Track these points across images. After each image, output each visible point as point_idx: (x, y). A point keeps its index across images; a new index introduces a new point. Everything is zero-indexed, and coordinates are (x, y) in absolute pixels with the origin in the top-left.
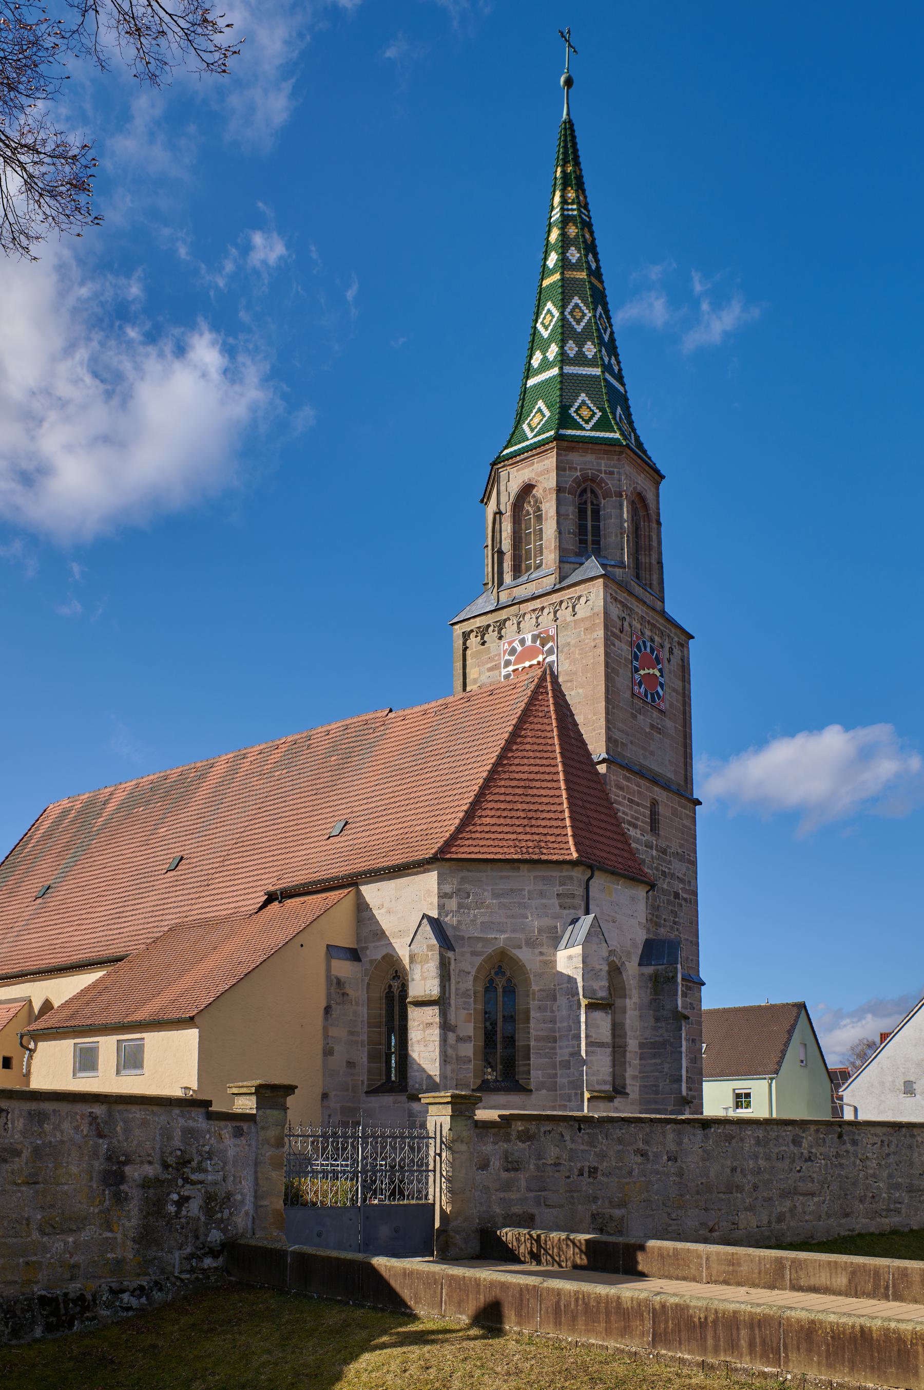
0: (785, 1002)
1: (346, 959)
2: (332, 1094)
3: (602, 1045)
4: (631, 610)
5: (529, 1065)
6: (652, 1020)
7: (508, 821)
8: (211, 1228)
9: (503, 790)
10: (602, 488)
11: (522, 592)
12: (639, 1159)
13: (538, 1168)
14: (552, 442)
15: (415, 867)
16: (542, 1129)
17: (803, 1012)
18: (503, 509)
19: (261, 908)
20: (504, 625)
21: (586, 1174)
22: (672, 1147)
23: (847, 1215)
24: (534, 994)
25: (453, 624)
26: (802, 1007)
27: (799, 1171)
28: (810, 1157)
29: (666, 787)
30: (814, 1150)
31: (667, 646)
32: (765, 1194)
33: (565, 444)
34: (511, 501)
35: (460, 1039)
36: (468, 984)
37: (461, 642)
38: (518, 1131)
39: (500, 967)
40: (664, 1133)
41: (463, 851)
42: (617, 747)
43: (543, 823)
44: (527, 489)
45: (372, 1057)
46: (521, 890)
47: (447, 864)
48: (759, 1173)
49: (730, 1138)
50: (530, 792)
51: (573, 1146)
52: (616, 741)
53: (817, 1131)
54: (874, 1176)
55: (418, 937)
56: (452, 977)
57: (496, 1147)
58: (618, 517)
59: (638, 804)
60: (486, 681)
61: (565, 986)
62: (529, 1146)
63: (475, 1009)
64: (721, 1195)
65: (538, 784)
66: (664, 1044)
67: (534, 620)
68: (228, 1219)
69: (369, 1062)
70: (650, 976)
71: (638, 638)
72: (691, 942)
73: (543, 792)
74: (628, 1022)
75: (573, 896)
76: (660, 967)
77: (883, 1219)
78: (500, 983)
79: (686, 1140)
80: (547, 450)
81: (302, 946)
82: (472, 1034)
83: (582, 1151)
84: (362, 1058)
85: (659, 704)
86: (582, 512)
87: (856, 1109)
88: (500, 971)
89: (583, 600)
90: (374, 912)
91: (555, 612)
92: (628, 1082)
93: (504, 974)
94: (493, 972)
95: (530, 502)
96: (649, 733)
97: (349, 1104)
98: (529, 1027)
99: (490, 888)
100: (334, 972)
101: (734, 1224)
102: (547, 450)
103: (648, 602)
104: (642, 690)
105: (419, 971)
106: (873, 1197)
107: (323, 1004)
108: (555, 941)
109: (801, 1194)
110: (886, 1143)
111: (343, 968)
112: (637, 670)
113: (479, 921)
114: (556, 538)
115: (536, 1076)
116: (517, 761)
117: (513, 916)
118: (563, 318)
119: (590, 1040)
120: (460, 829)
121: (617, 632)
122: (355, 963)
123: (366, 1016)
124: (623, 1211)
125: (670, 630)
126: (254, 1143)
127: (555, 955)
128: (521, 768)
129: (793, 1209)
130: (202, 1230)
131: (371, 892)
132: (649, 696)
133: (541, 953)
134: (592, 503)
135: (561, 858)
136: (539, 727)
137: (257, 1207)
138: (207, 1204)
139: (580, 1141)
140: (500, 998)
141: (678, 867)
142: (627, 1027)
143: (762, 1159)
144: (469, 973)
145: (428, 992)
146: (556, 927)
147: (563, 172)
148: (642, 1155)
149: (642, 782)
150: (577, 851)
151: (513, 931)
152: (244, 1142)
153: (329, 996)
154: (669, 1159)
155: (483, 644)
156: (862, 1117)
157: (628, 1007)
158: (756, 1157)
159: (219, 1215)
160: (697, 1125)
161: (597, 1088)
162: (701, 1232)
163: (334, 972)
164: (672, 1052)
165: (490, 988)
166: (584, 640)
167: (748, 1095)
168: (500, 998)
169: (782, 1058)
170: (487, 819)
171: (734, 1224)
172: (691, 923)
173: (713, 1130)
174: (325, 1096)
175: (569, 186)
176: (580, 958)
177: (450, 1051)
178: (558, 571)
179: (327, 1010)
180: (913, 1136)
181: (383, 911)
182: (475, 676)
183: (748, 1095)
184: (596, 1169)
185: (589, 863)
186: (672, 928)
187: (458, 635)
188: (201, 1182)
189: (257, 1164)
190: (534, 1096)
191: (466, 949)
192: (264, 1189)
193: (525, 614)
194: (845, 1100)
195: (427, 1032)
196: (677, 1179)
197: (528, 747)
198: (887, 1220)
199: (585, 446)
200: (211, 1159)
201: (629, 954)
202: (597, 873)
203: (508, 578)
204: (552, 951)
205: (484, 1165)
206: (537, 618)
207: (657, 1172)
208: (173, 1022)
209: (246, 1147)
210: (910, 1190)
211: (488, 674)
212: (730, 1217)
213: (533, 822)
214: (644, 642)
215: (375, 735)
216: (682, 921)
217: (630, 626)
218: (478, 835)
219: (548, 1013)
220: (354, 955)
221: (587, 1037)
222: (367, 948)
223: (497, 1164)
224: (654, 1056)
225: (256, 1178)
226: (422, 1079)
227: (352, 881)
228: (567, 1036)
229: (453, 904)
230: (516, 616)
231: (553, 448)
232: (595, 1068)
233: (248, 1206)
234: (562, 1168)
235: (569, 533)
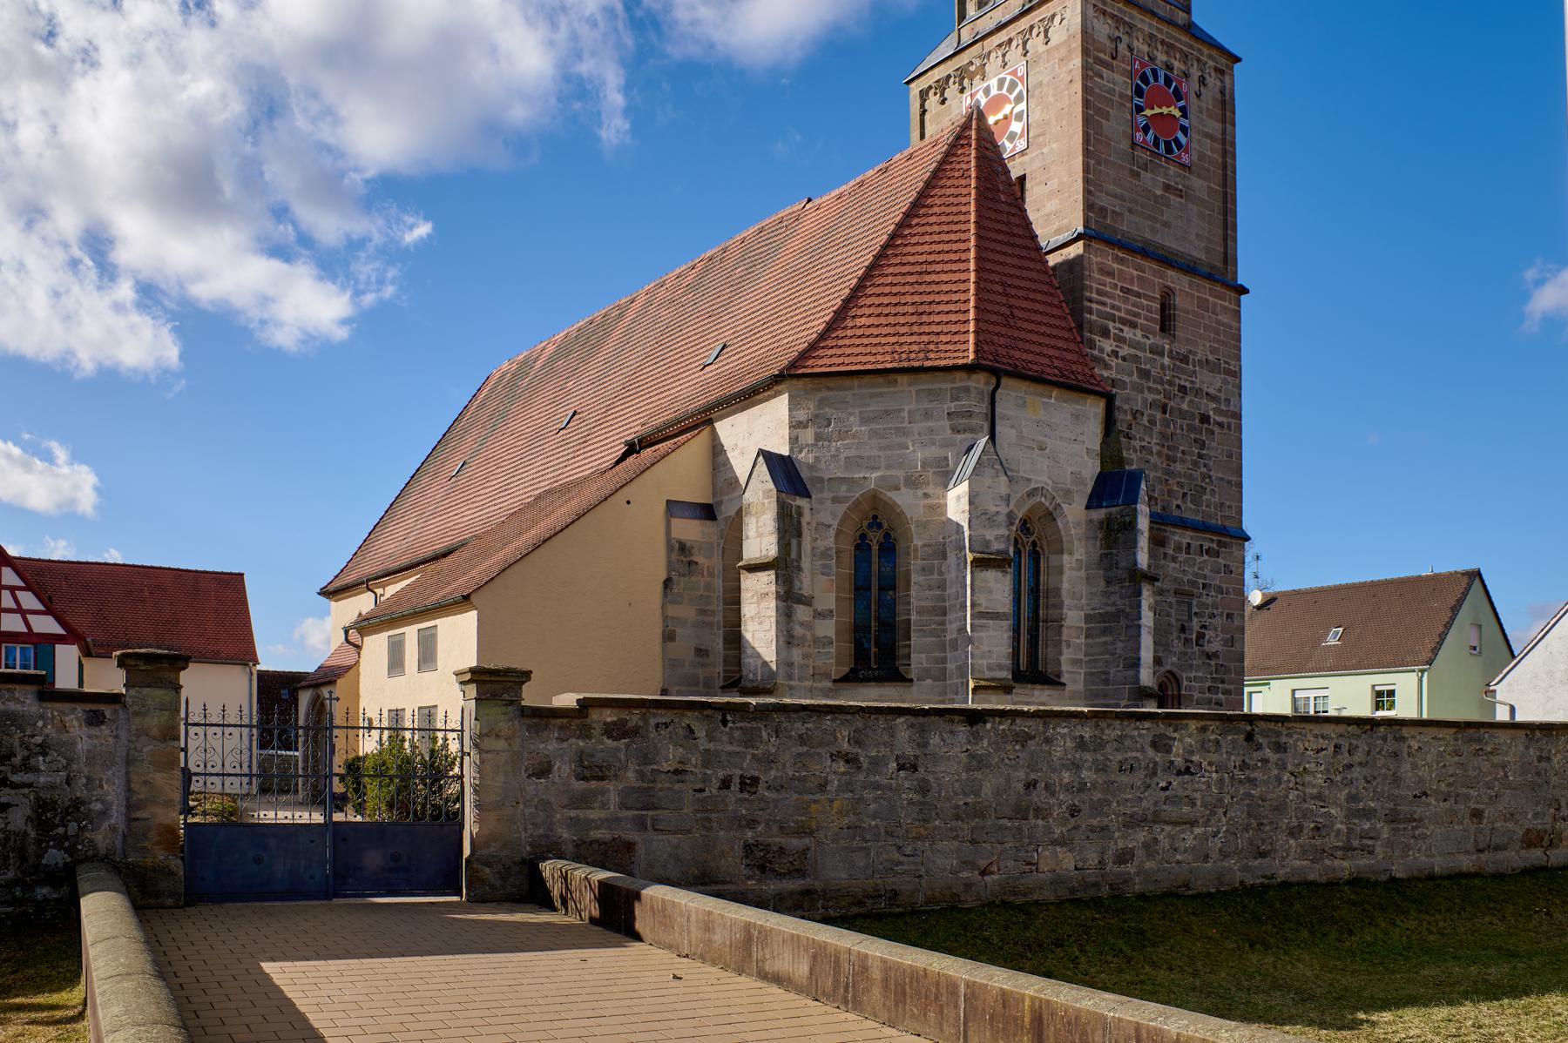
0: (1452, 570)
3: (995, 616)
4: (1131, 26)
6: (1103, 583)
7: (891, 320)
8: (48, 847)
9: (889, 280)
11: (987, 24)
12: (841, 767)
13: (641, 775)
16: (653, 722)
17: (1477, 581)
19: (617, 463)
21: (735, 786)
22: (910, 751)
23: (1263, 855)
24: (916, 550)
26: (1476, 575)
27: (1164, 789)
28: (1188, 768)
29: (1189, 268)
30: (1196, 758)
31: (1195, 73)
32: (1095, 822)
35: (818, 615)
36: (829, 541)
37: (918, 105)
38: (605, 723)
39: (875, 517)
40: (891, 731)
41: (819, 365)
42: (1105, 217)
43: (937, 319)
46: (899, 411)
47: (800, 383)
48: (1080, 790)
49: (1024, 739)
50: (928, 278)
51: (711, 746)
52: (1103, 210)
53: (1204, 729)
54: (1319, 797)
56: (805, 532)
57: (565, 745)
59: (1138, 295)
62: (627, 746)
63: (838, 574)
64: (1005, 821)
65: (938, 268)
66: (1116, 616)
68: (77, 835)
70: (1101, 523)
71: (1143, 65)
72: (1229, 482)
73: (944, 277)
74: (1065, 586)
75: (970, 414)
76: (1113, 510)
77: (1337, 862)
78: (875, 539)
79: (935, 740)
82: (833, 607)
83: (730, 754)
85: (1179, 157)
87: (1512, 709)
88: (875, 523)
89: (1057, 19)
92: (1064, 668)
93: (880, 526)
94: (865, 523)
96: (1162, 196)
99: (857, 411)
100: (675, 534)
101: (1029, 864)
103: (1162, 13)
104: (1150, 137)
106: (1317, 829)
107: (664, 576)
108: (945, 477)
109: (1168, 823)
110: (1345, 749)
111: (690, 530)
112: (1139, 109)
113: (842, 456)
116: (914, 240)
117: (888, 447)
119: (977, 609)
120: (822, 336)
121: (1107, 58)
124: (807, 840)
125: (1200, 51)
126: (123, 735)
127: (944, 497)
128: (919, 248)
129: (1150, 847)
130: (32, 848)
132: (1162, 146)
135: (951, 362)
136: (953, 191)
137: (130, 820)
138: (39, 815)
139: (724, 738)
140: (875, 558)
141: (1208, 381)
142: (1064, 594)
143: (1090, 769)
146: (946, 458)
148: (847, 762)
149: (1146, 264)
150: (976, 352)
151: (888, 467)
152: (107, 732)
153: (670, 567)
154: (901, 768)
155: (943, 102)
156: (1519, 718)
157: (1067, 566)
158: (1076, 766)
159: (61, 830)
160: (957, 718)
161: (988, 675)
162: (964, 875)
163: (675, 534)
164: (1128, 627)
165: (862, 546)
167: (1391, 693)
168: (875, 558)
169: (1440, 643)
171: (1029, 864)
172: (1230, 456)
173: (989, 726)
177: (798, 631)
179: (667, 583)
180: (1402, 739)
183: (1391, 693)
184: (755, 781)
185: (994, 367)
186: (1195, 463)
188: (29, 785)
189: (129, 762)
190: (914, 689)
191: (827, 494)
192: (142, 796)
194: (1499, 697)
196: (916, 797)
197: (933, 219)
198: (1345, 864)
200: (45, 754)
201: (1068, 493)
202: (1004, 381)
204: (939, 491)
205: (543, 771)
207: (877, 786)
208: (456, 603)
209: (111, 740)
210: (1393, 818)
212: (1022, 854)
213: (925, 318)
214: (1154, 72)
216: (1212, 453)
217: (1130, 49)
218: (847, 342)
221: (973, 605)
223: (566, 769)
224: (1104, 632)
225: (128, 782)
227: (703, 419)
229: (808, 436)
232: (985, 648)
233: (116, 818)
234: (688, 777)
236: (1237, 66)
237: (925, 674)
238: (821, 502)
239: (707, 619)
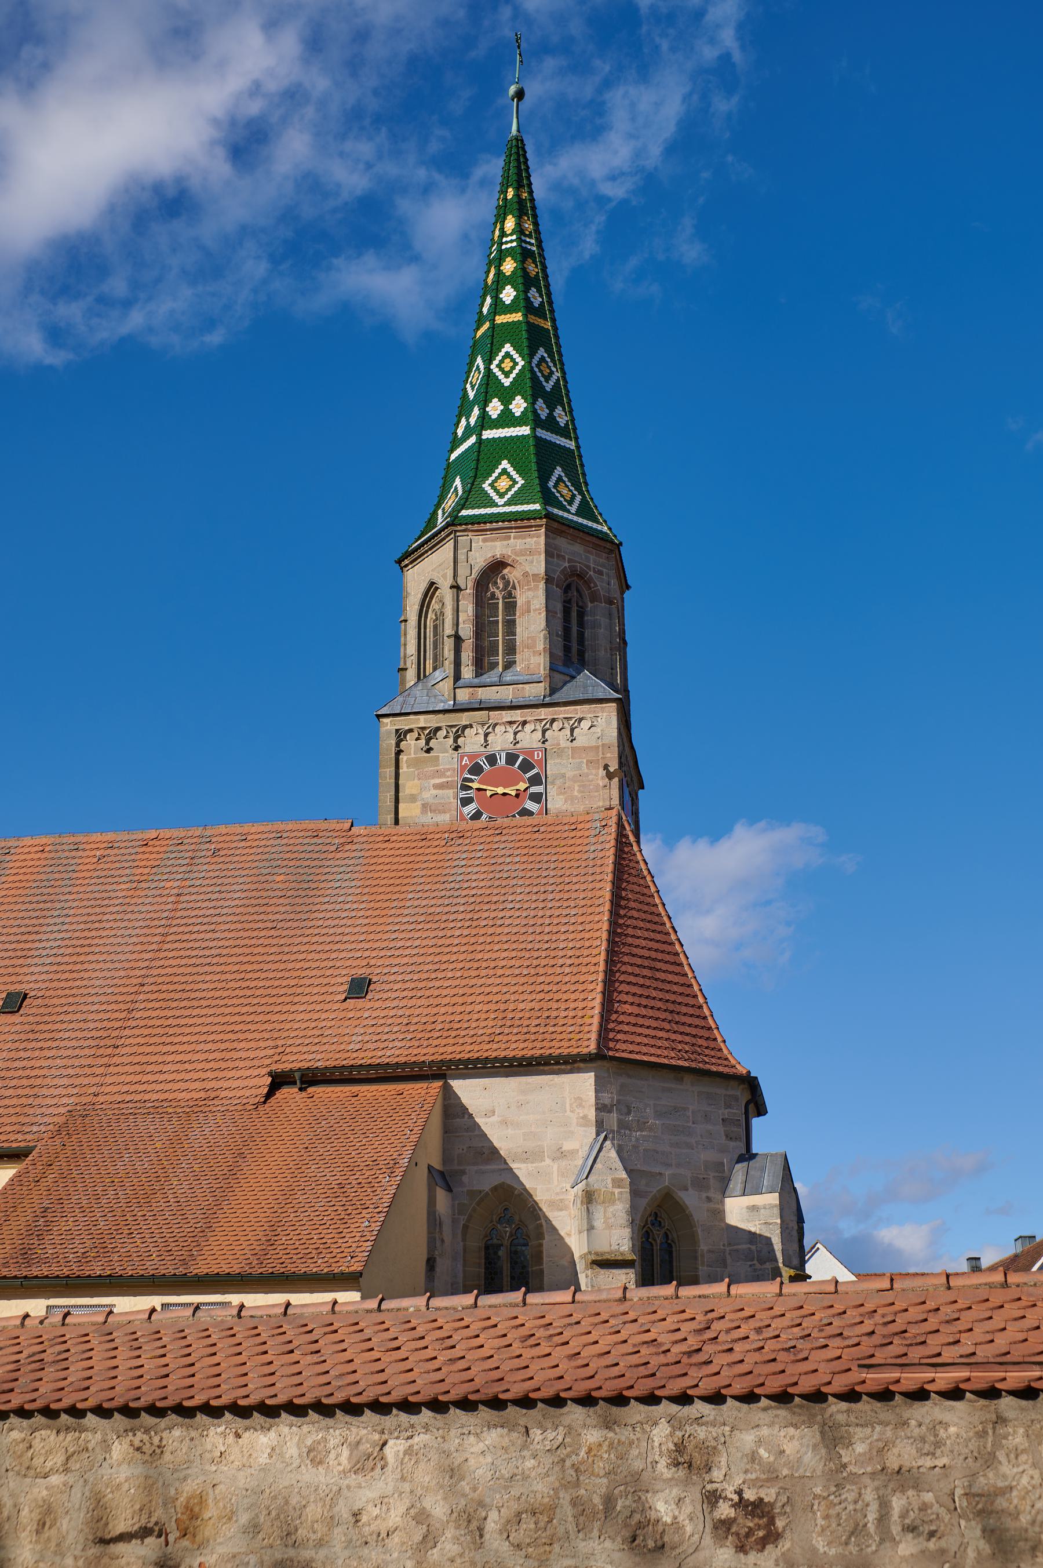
10: (590, 588)
14: (541, 518)
18: (461, 583)
19: (269, 1095)
24: (703, 1256)
33: (555, 525)
44: (497, 567)
46: (686, 1109)
55: (598, 1166)
60: (431, 801)
61: (745, 1246)
67: (539, 734)
80: (531, 526)
86: (567, 612)
89: (585, 724)
91: (544, 732)
99: (652, 1103)
102: (531, 526)
118: (529, 368)
123: (461, 1275)
127: (723, 1203)
131: (458, 1085)
133: (709, 1199)
145: (614, 1247)
146: (723, 1163)
147: (517, 195)
155: (429, 750)
166: (587, 775)
170: (627, 1006)
175: (526, 214)
181: (494, 1119)
182: (414, 791)
187: (389, 732)
193: (496, 724)
199: (576, 533)
203: (467, 672)
206: (516, 733)
211: (435, 792)
215: (339, 855)
222: (463, 1172)
227: (439, 1072)
230: (483, 725)
231: (541, 526)
235: (557, 635)
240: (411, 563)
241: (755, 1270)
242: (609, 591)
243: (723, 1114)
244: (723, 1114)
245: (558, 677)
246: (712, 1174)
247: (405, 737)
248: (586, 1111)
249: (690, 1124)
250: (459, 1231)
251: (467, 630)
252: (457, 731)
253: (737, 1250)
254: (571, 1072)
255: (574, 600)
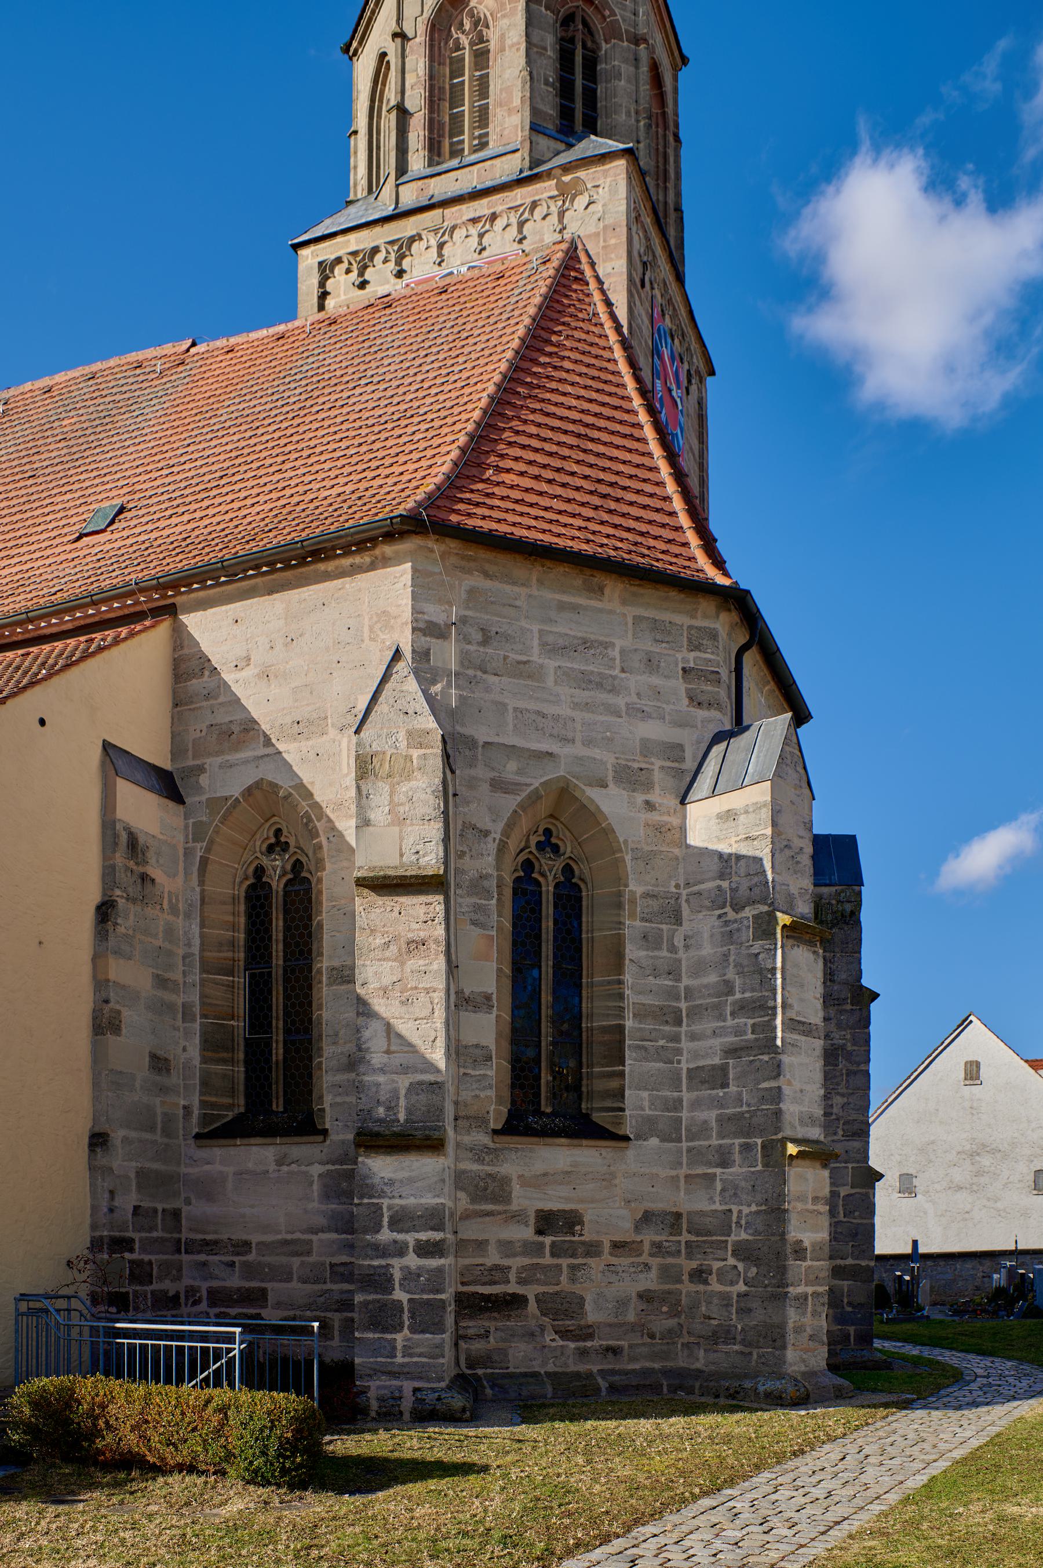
1: (151, 789)
2: (118, 1135)
5: (622, 1074)
10: (604, 18)
15: (347, 553)
18: (408, 29)
20: (409, 248)
24: (633, 902)
25: (296, 247)
34: (426, 15)
37: (315, 281)
39: (548, 832)
45: (214, 1044)
46: (607, 645)
58: (623, 87)
67: (474, 241)
69: (204, 1060)
81: (42, 722)
84: (188, 1051)
88: (548, 844)
90: (225, 676)
91: (521, 225)
94: (534, 840)
95: (462, 24)
97: (155, 1166)
98: (620, 982)
105: (385, 799)
107: (95, 897)
111: (141, 809)
114: (524, 83)
115: (638, 1103)
117: (587, 706)
122: (171, 804)
123: (197, 942)
133: (650, 806)
134: (584, 47)
144: (486, 833)
145: (409, 858)
151: (588, 743)
153: (109, 875)
170: (512, 476)
174: (98, 1140)
176: (766, 814)
178: (527, 144)
179: (105, 911)
181: (248, 673)
190: (631, 1153)
191: (480, 772)
193: (454, 228)
195: (413, 964)
203: (417, 162)
206: (481, 236)
219: (665, 953)
220: (168, 785)
222: (201, 769)
226: (395, 1093)
227: (157, 601)
228: (718, 1007)
230: (436, 231)
235: (547, 83)
236: (710, 380)
237: (649, 1128)
238: (472, 784)
239: (169, 997)
240: (360, 43)
241: (727, 923)
242: (636, 25)
243: (685, 660)
244: (685, 660)
245: (543, 142)
246: (658, 763)
247: (332, 271)
248: (396, 636)
249: (616, 672)
250: (195, 869)
251: (416, 100)
252: (401, 247)
253: (699, 893)
254: (372, 567)
255: (579, 36)
